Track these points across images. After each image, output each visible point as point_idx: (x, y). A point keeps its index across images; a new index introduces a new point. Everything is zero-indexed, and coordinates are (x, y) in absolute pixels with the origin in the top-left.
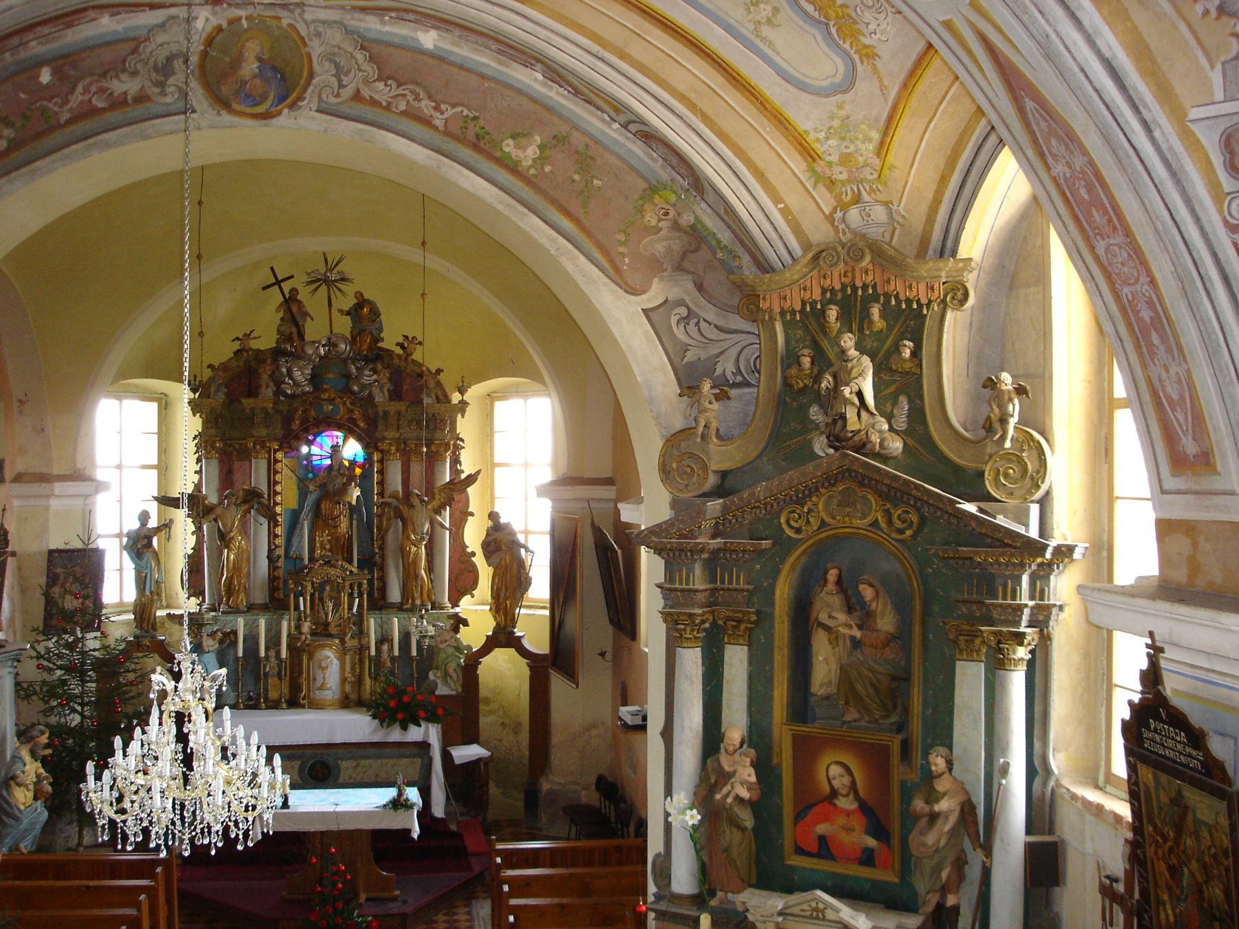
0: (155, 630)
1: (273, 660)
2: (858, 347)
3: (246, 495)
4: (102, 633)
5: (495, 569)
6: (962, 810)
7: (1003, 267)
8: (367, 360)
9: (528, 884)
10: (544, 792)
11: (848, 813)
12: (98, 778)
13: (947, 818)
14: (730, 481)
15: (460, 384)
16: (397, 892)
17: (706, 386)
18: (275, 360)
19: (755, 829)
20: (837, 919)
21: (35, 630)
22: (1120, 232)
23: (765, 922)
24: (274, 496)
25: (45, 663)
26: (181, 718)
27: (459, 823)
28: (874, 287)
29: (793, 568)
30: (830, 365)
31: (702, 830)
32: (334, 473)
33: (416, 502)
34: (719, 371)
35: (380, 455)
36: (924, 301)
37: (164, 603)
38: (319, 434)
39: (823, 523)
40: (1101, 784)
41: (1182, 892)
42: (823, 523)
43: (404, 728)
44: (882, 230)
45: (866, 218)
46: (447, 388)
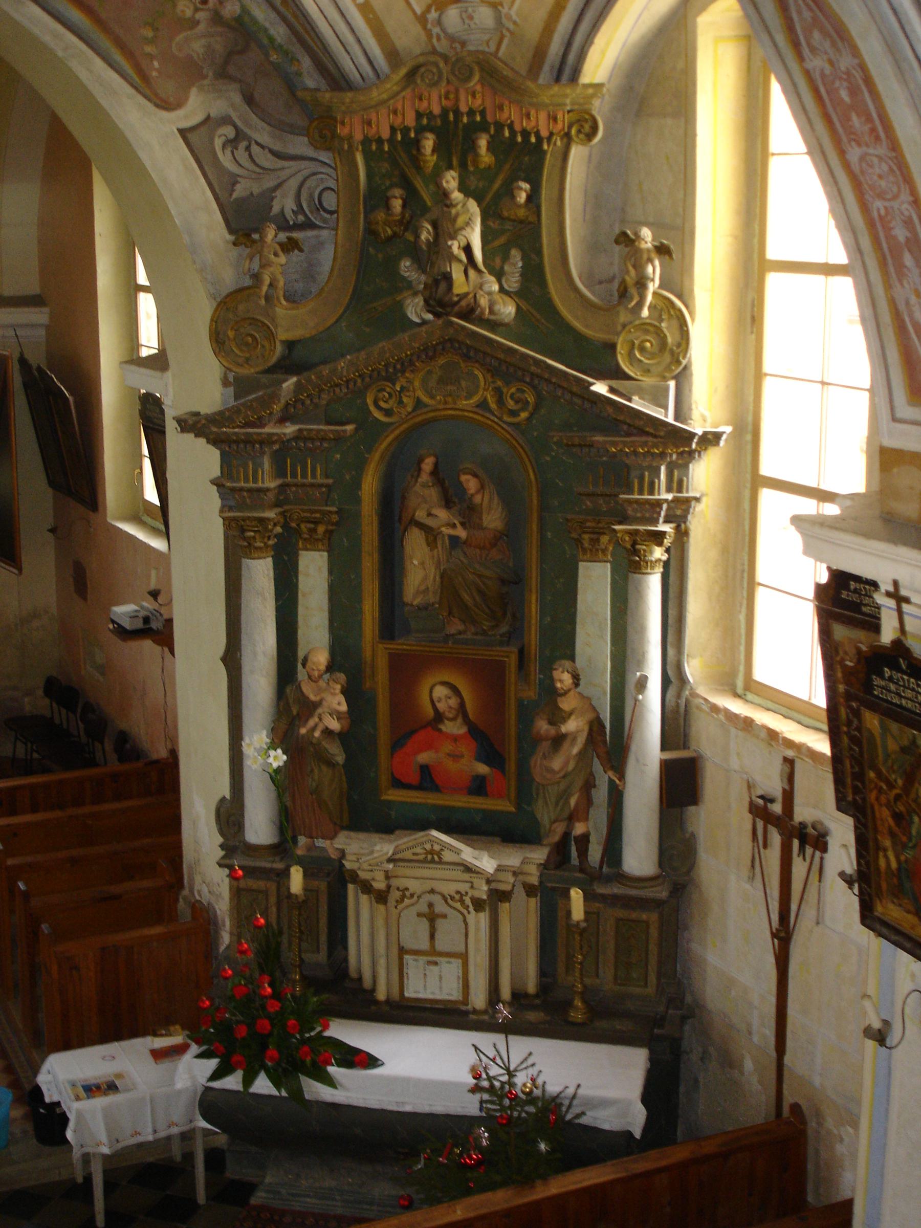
2: (462, 188)
6: (591, 730)
7: (632, 88)
11: (455, 739)
13: (574, 739)
20: (461, 861)
22: (884, 143)
28: (483, 113)
29: (382, 457)
30: (425, 210)
36: (544, 133)
39: (418, 403)
40: (740, 690)
41: (910, 839)
42: (418, 403)
44: (486, 37)
45: (467, 21)
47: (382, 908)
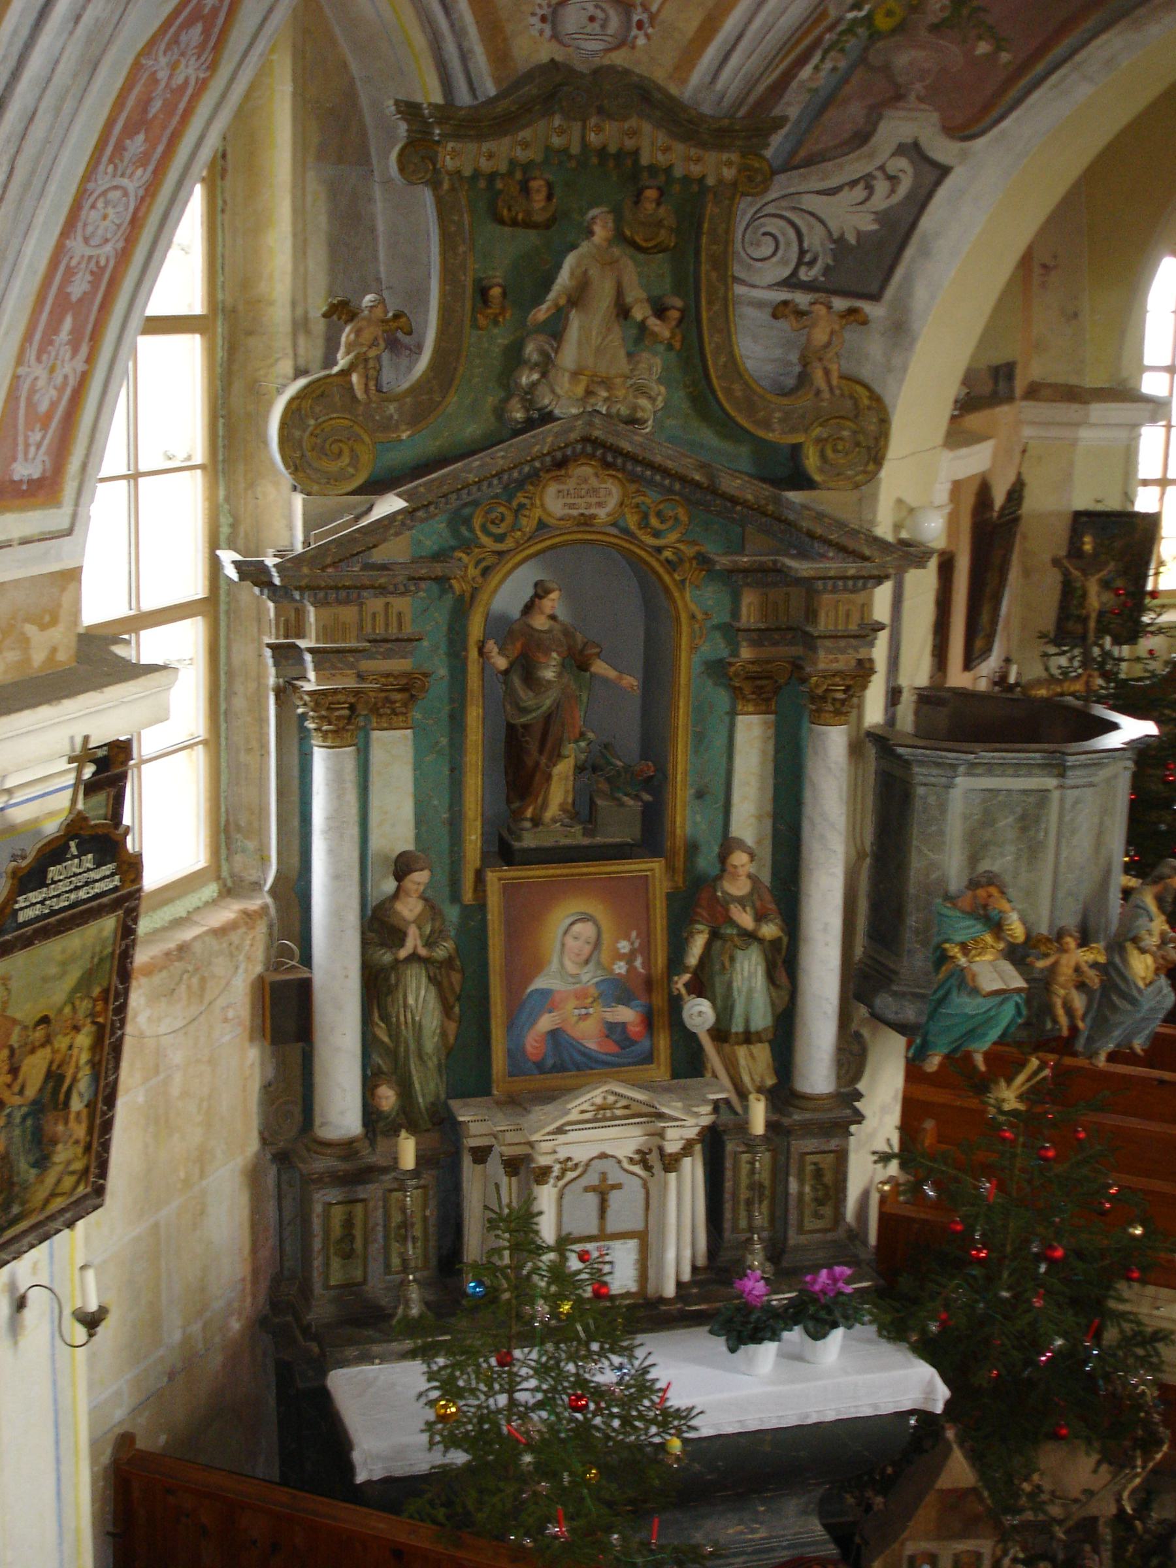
21: (1042, 636)
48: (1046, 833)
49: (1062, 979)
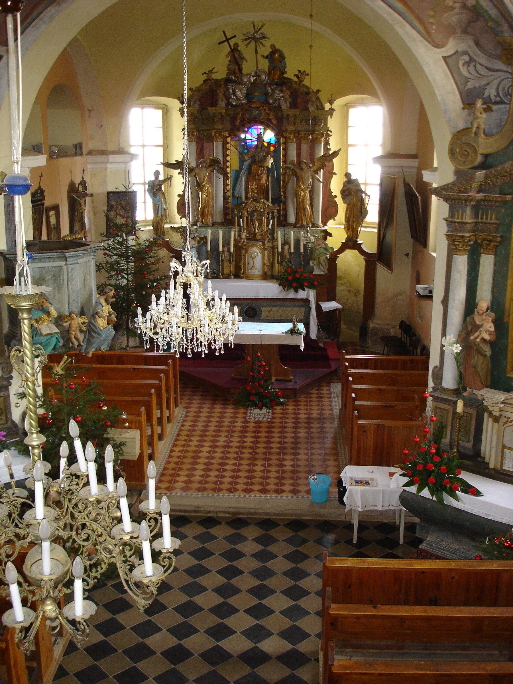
0: (164, 235)
1: (226, 252)
3: (211, 162)
4: (137, 237)
5: (348, 205)
8: (277, 84)
9: (362, 377)
10: (370, 328)
12: (144, 315)
14: (490, 160)
15: (330, 99)
16: (292, 377)
17: (479, 104)
18: (226, 85)
19: (492, 356)
21: (102, 234)
23: (493, 406)
24: (226, 163)
25: (108, 252)
26: (186, 286)
27: (324, 343)
31: (462, 355)
32: (259, 150)
33: (304, 167)
34: (486, 94)
35: (284, 140)
37: (168, 221)
38: (249, 128)
43: (296, 291)
46: (323, 100)
47: (496, 424)
48: (63, 280)
49: (73, 329)
